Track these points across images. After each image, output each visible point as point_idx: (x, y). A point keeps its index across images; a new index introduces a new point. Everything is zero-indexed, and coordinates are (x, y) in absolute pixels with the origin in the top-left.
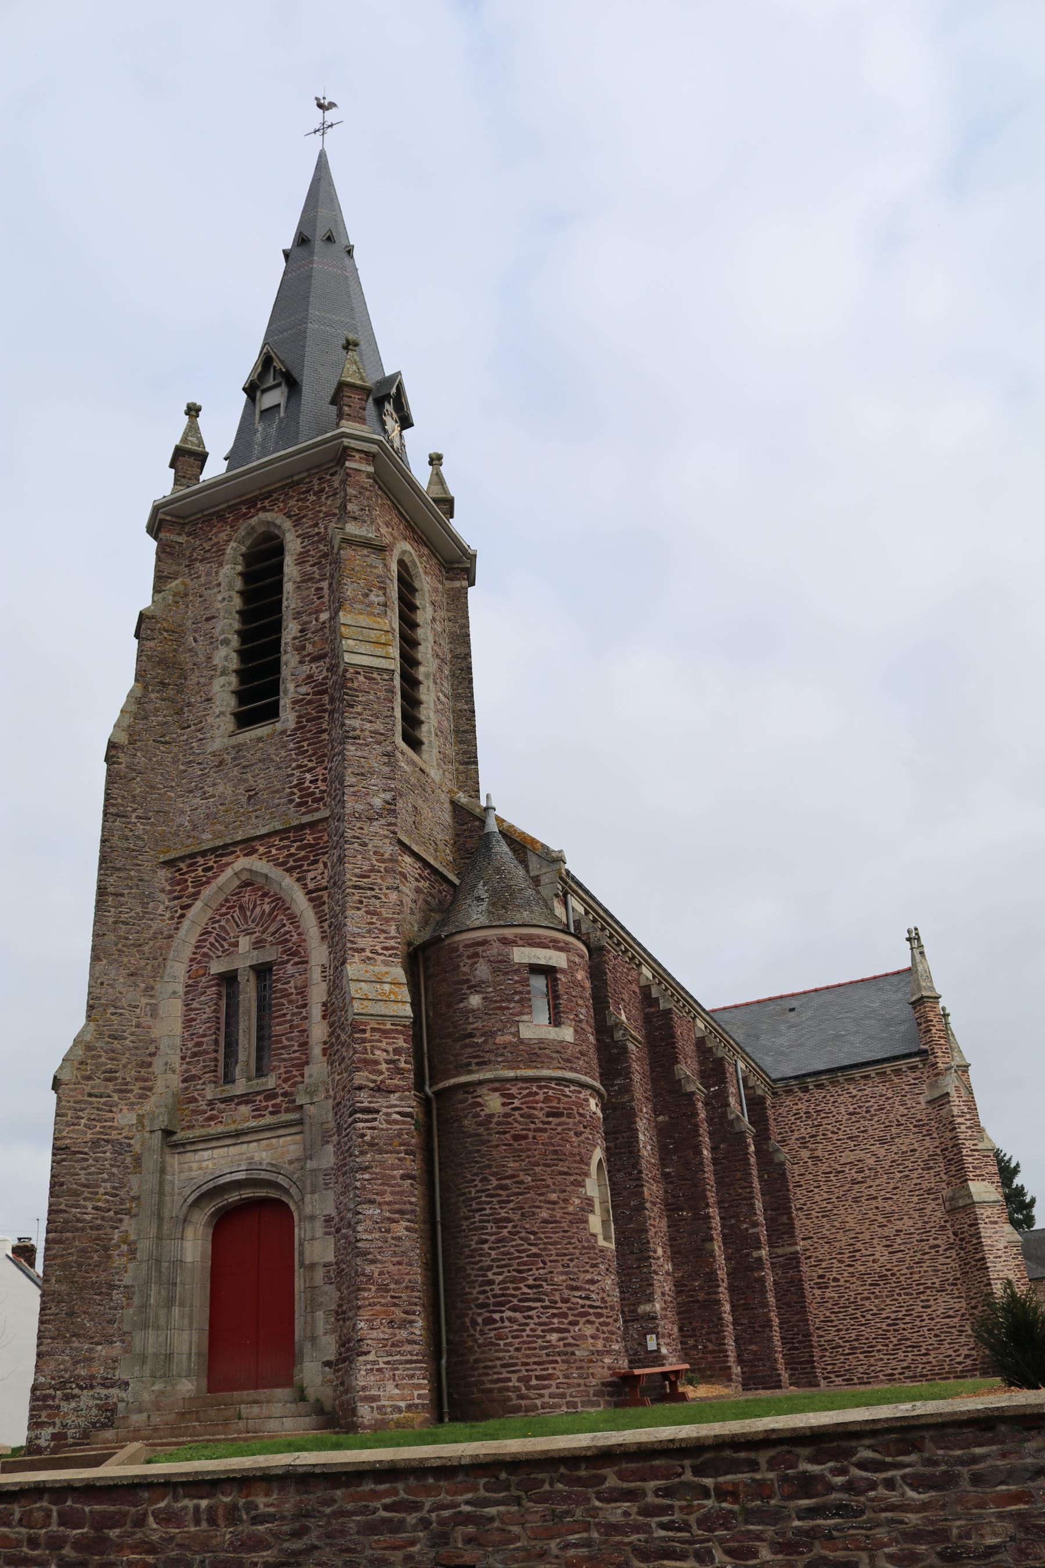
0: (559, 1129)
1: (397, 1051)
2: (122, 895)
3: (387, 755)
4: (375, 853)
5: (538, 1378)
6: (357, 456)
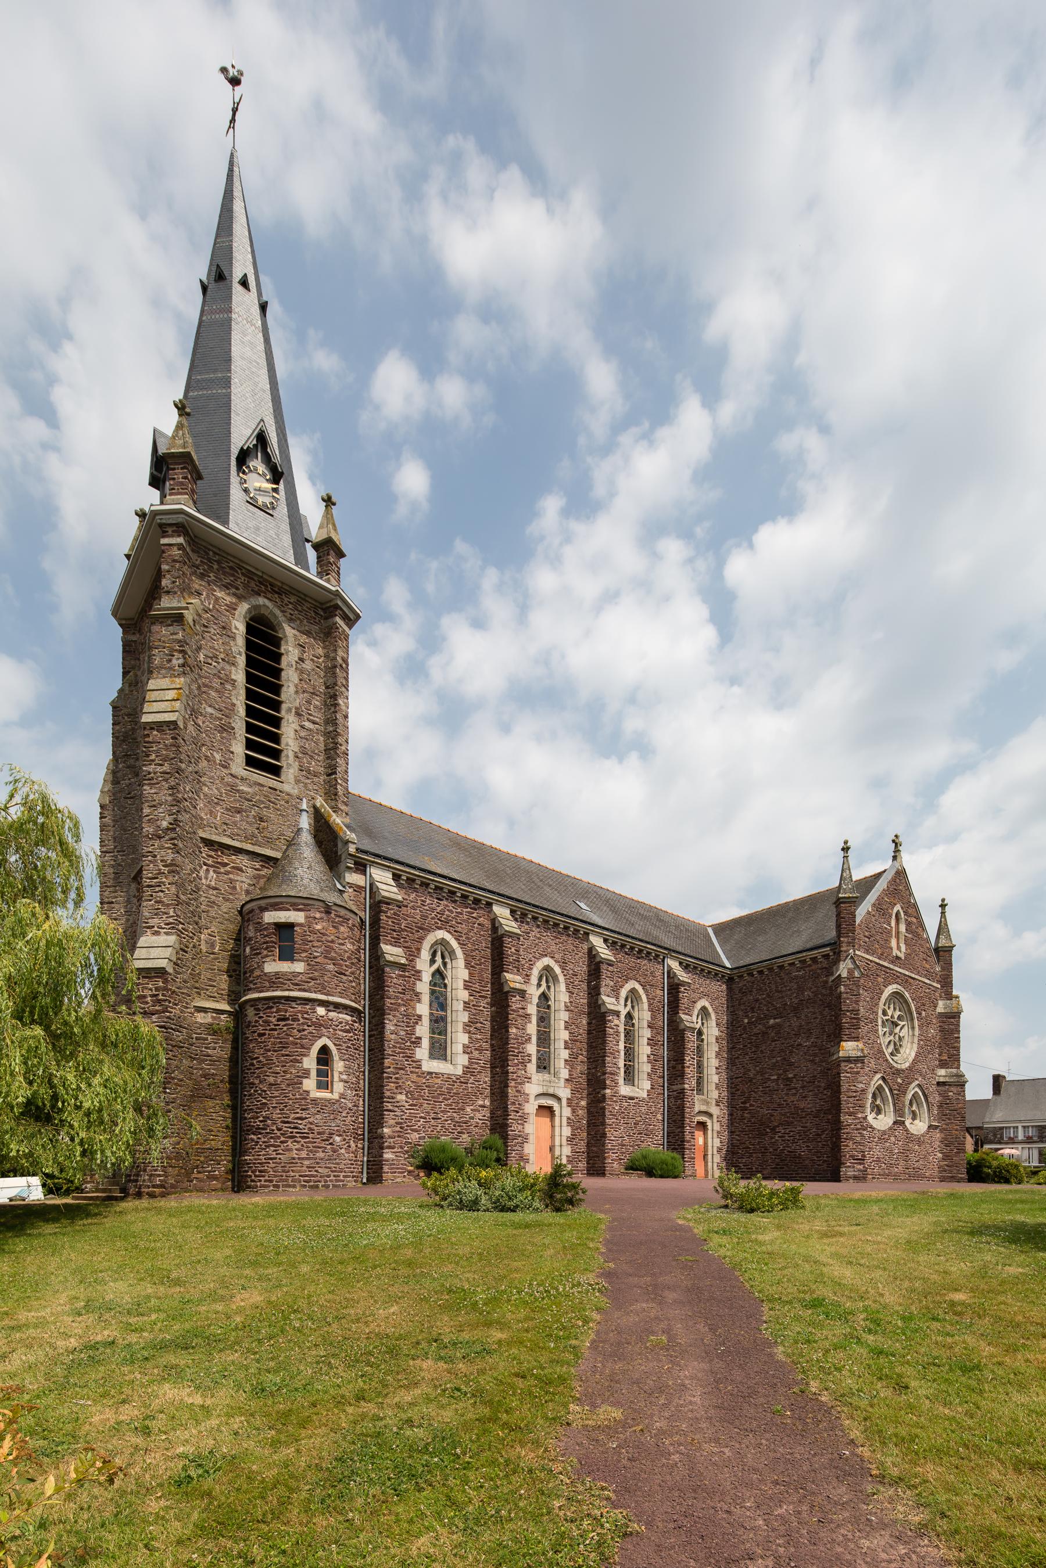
0: (285, 1028)
1: (157, 989)
2: (112, 903)
3: (171, 788)
4: (162, 861)
5: (260, 1171)
6: (170, 530)
